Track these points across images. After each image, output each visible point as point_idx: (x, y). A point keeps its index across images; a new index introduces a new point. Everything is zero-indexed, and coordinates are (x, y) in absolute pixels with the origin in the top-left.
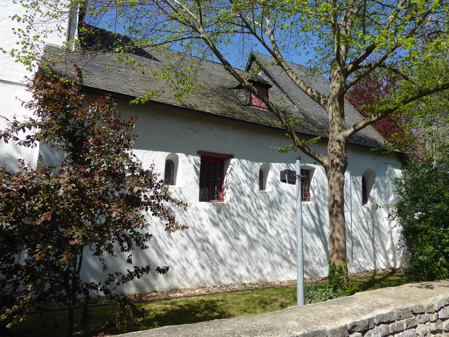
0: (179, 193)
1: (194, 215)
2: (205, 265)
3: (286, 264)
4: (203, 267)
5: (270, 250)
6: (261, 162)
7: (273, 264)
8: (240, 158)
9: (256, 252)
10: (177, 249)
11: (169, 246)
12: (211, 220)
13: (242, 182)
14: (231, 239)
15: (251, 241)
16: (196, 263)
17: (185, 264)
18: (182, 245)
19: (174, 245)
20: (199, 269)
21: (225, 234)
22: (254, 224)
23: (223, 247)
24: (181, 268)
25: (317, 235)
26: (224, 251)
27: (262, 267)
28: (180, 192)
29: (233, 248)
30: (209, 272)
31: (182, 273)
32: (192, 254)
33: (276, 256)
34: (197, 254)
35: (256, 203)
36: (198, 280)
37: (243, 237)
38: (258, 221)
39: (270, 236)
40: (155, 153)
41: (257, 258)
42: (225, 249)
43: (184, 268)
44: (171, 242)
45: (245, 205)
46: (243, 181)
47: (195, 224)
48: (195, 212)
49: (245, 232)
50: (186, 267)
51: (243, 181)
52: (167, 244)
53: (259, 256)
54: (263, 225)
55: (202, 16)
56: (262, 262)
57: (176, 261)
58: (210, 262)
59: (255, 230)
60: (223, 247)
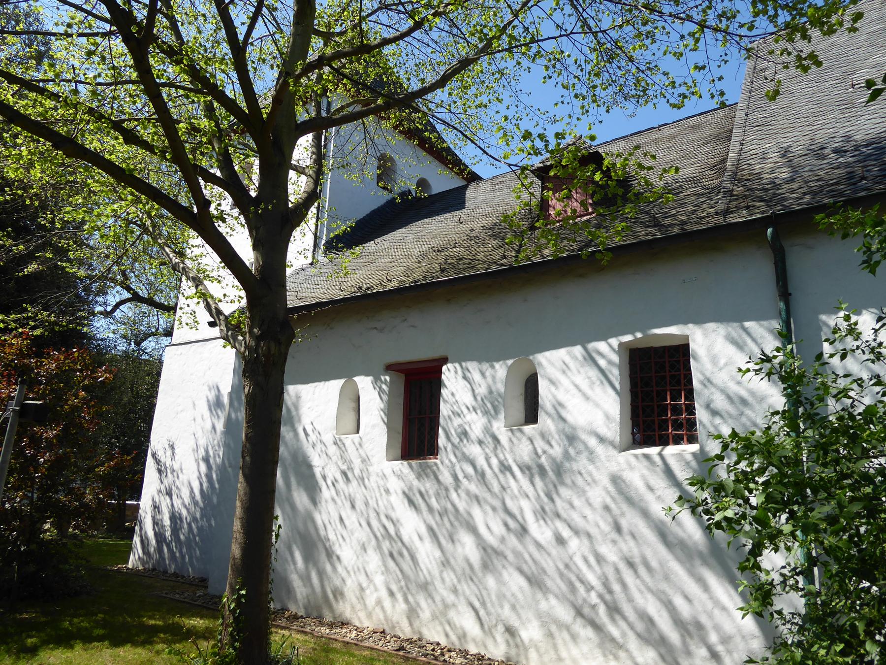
0: (358, 446)
1: (379, 487)
2: (394, 588)
3: (587, 633)
4: (391, 594)
5: (536, 581)
6: (508, 359)
7: (548, 622)
8: (460, 359)
9: (500, 581)
10: (352, 548)
11: (341, 540)
12: (404, 493)
13: (465, 411)
14: (443, 541)
15: (484, 549)
16: (379, 579)
17: (362, 579)
18: (359, 541)
19: (348, 540)
20: (384, 593)
21: (430, 529)
22: (494, 509)
23: (427, 553)
24: (356, 583)
25: (717, 574)
26: (429, 566)
27: (514, 622)
28: (360, 445)
29: (446, 563)
30: (402, 606)
31: (358, 593)
32: (374, 561)
33: (553, 601)
34: (380, 563)
35: (496, 456)
36: (381, 616)
37: (467, 541)
38: (504, 503)
39: (539, 545)
40: (327, 383)
41: (501, 597)
42: (431, 563)
43: (362, 589)
44: (345, 534)
45: (473, 464)
46: (468, 408)
47: (380, 503)
48: (381, 483)
49: (473, 530)
50: (364, 585)
51: (468, 408)
52: (339, 537)
53: (504, 589)
54: (516, 511)
55: (94, 11)
56: (513, 607)
57: (350, 568)
58: (403, 583)
59: (498, 528)
60: (427, 553)
